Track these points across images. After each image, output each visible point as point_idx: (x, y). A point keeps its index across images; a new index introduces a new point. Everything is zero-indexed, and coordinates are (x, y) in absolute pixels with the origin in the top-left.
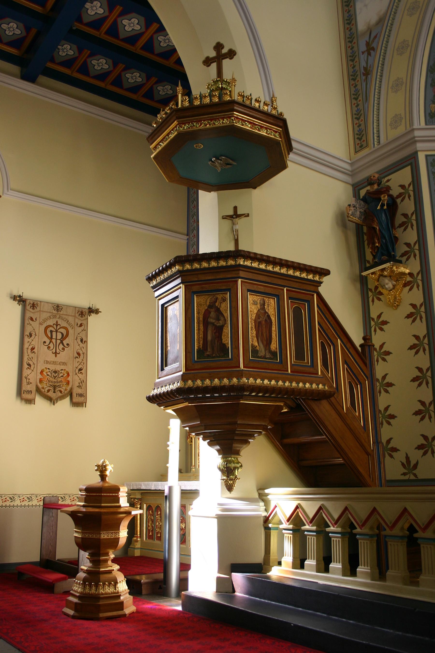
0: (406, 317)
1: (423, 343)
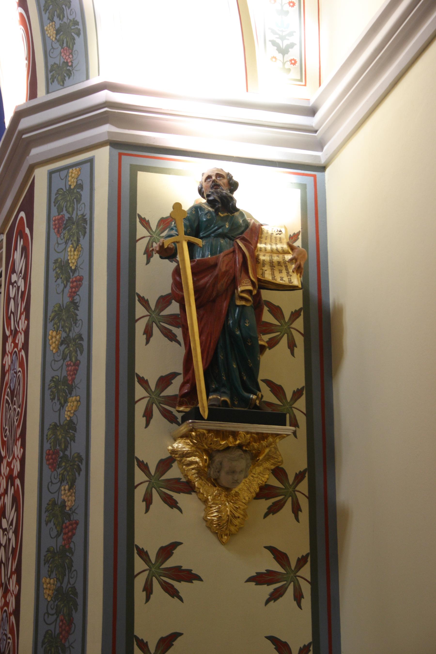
0: (250, 580)
1: (290, 328)
